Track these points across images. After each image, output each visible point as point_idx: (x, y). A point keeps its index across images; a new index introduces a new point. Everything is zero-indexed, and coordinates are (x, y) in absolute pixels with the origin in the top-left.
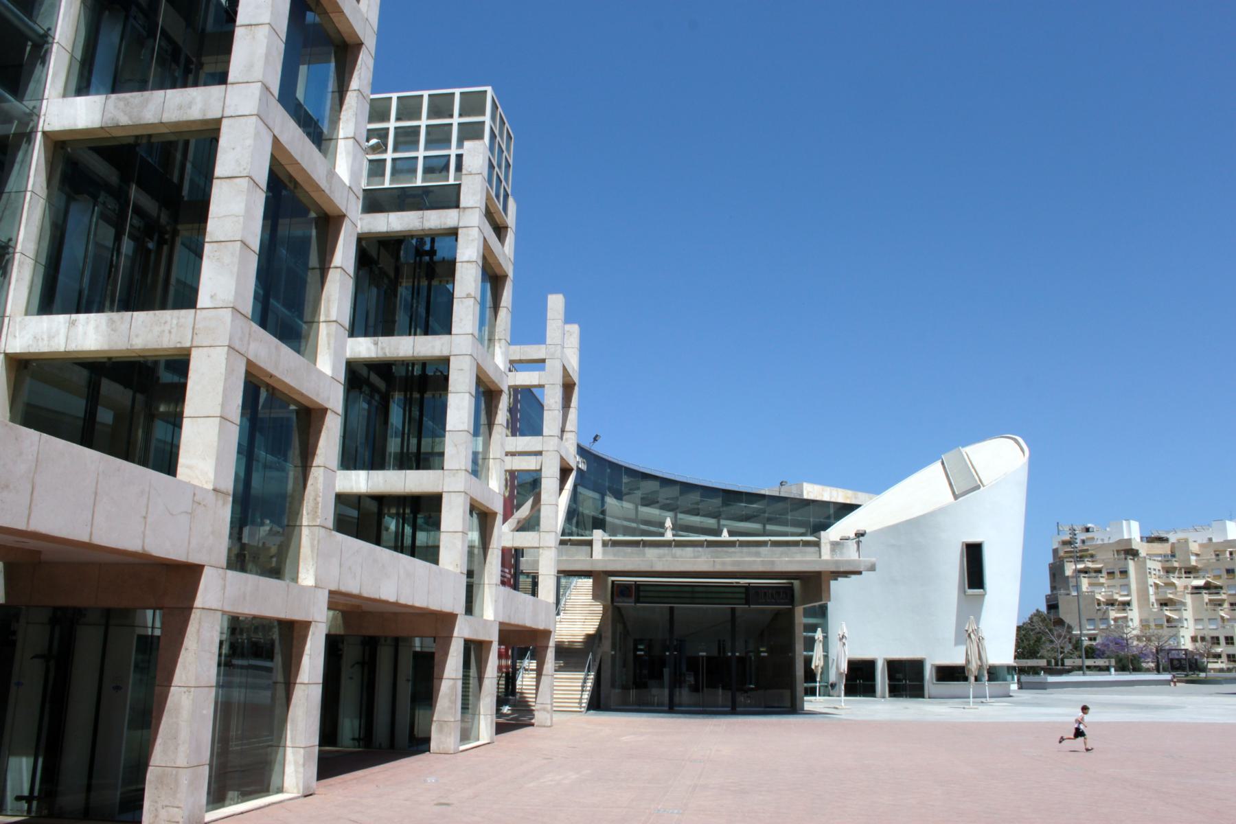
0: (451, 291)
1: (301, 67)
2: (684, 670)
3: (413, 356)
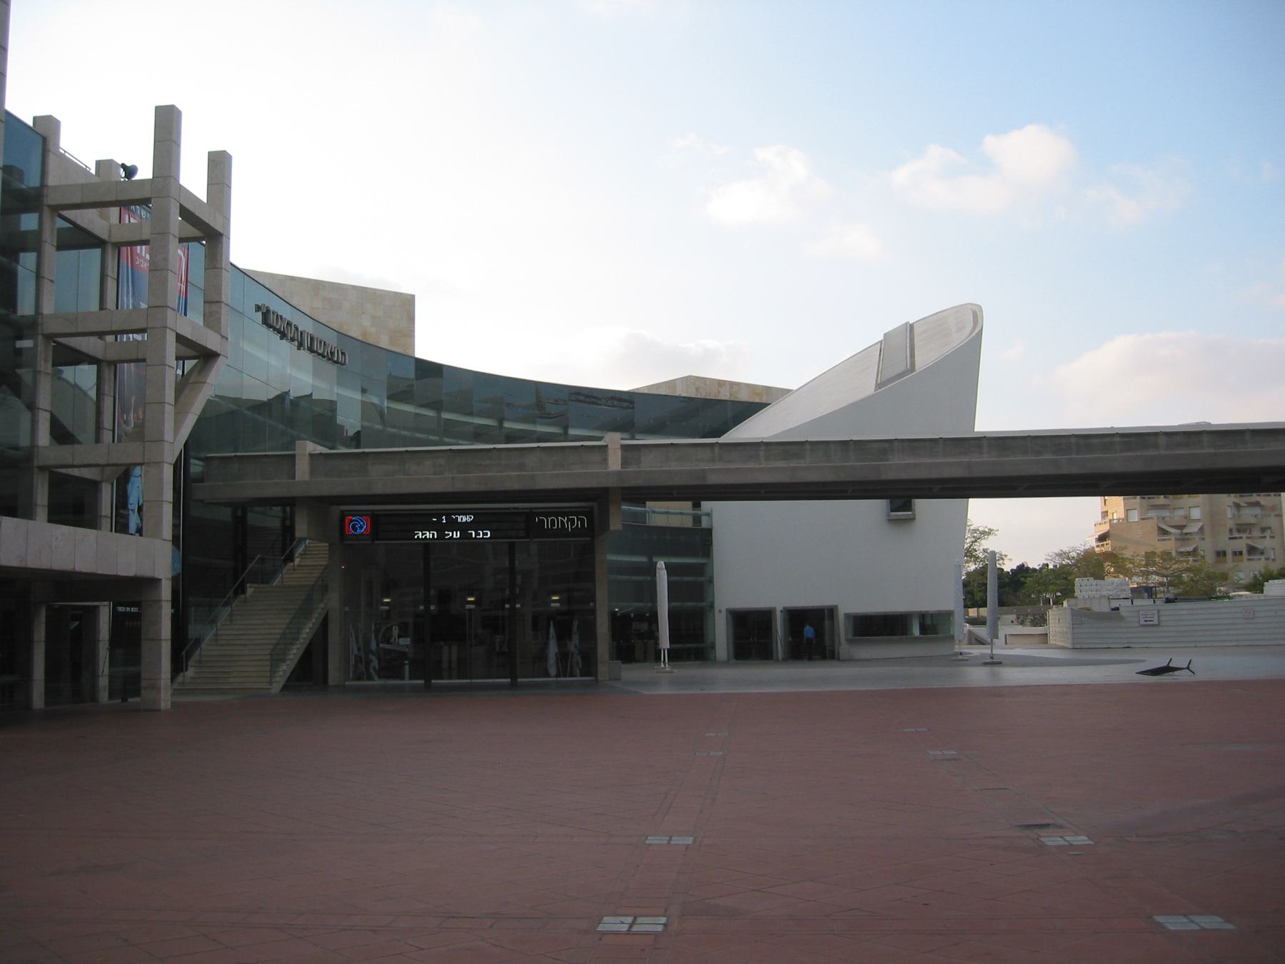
0: (1067, 844)
1: (307, 477)
2: (191, 643)
3: (99, 641)
